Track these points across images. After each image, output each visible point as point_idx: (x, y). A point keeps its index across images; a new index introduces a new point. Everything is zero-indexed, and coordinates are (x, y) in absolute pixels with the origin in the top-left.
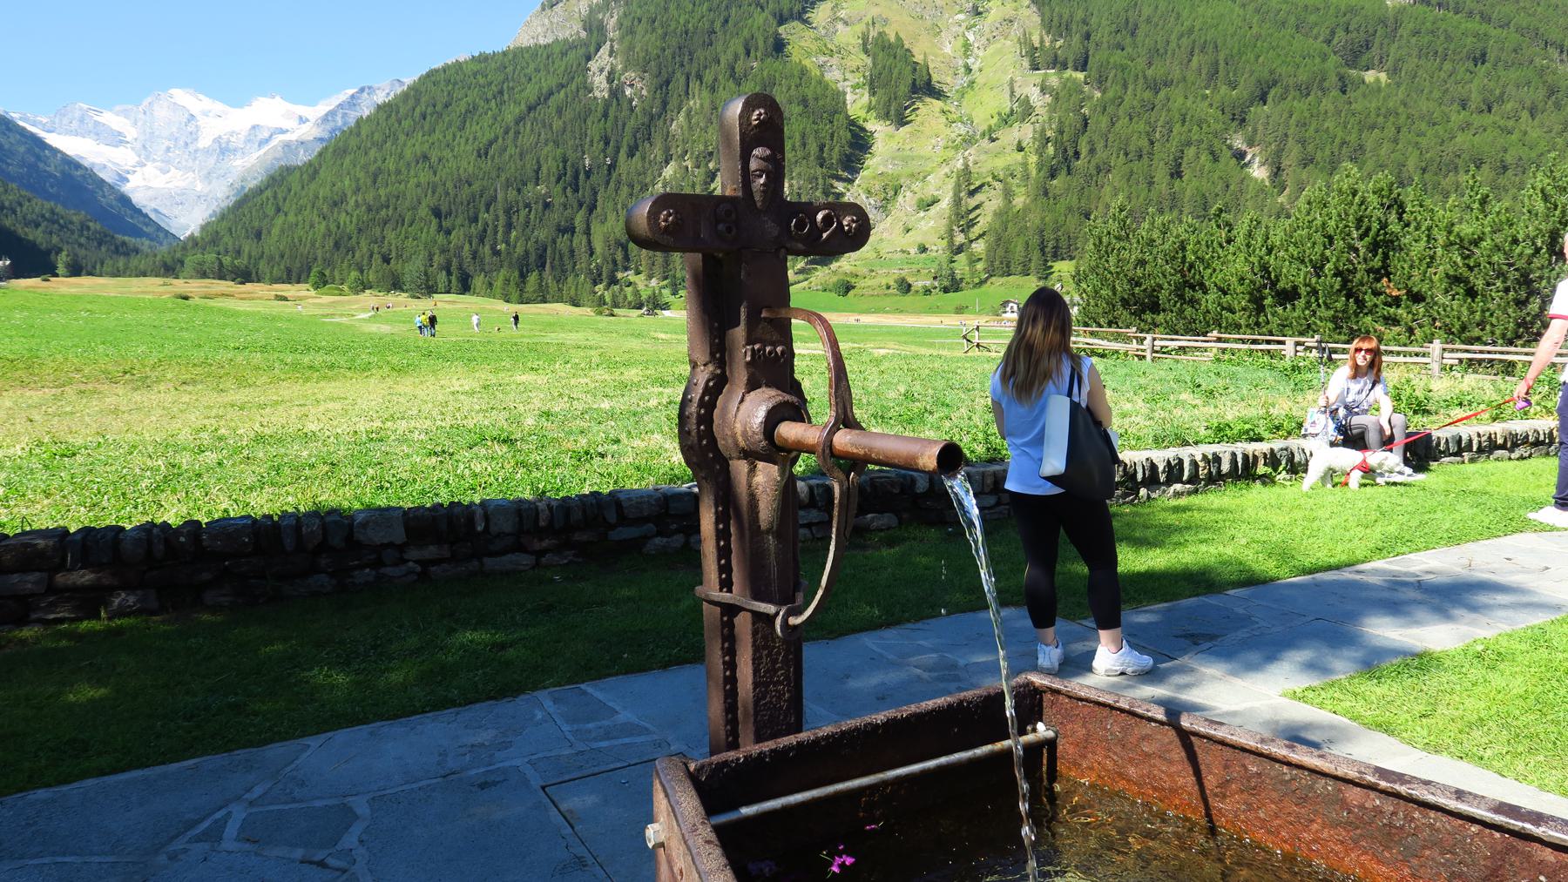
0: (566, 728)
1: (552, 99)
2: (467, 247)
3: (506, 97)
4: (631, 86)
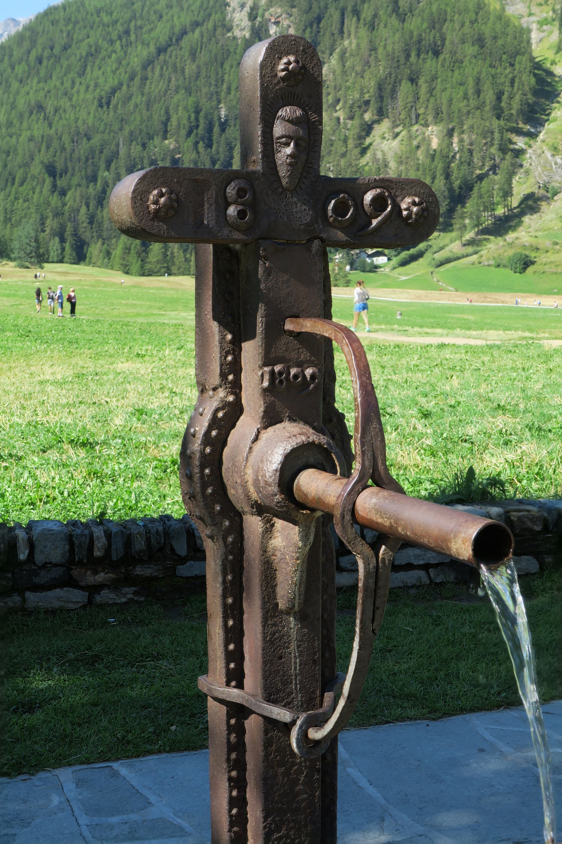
0: (84, 820)
1: (186, 39)
2: (83, 209)
3: (133, 37)
4: (277, 23)
